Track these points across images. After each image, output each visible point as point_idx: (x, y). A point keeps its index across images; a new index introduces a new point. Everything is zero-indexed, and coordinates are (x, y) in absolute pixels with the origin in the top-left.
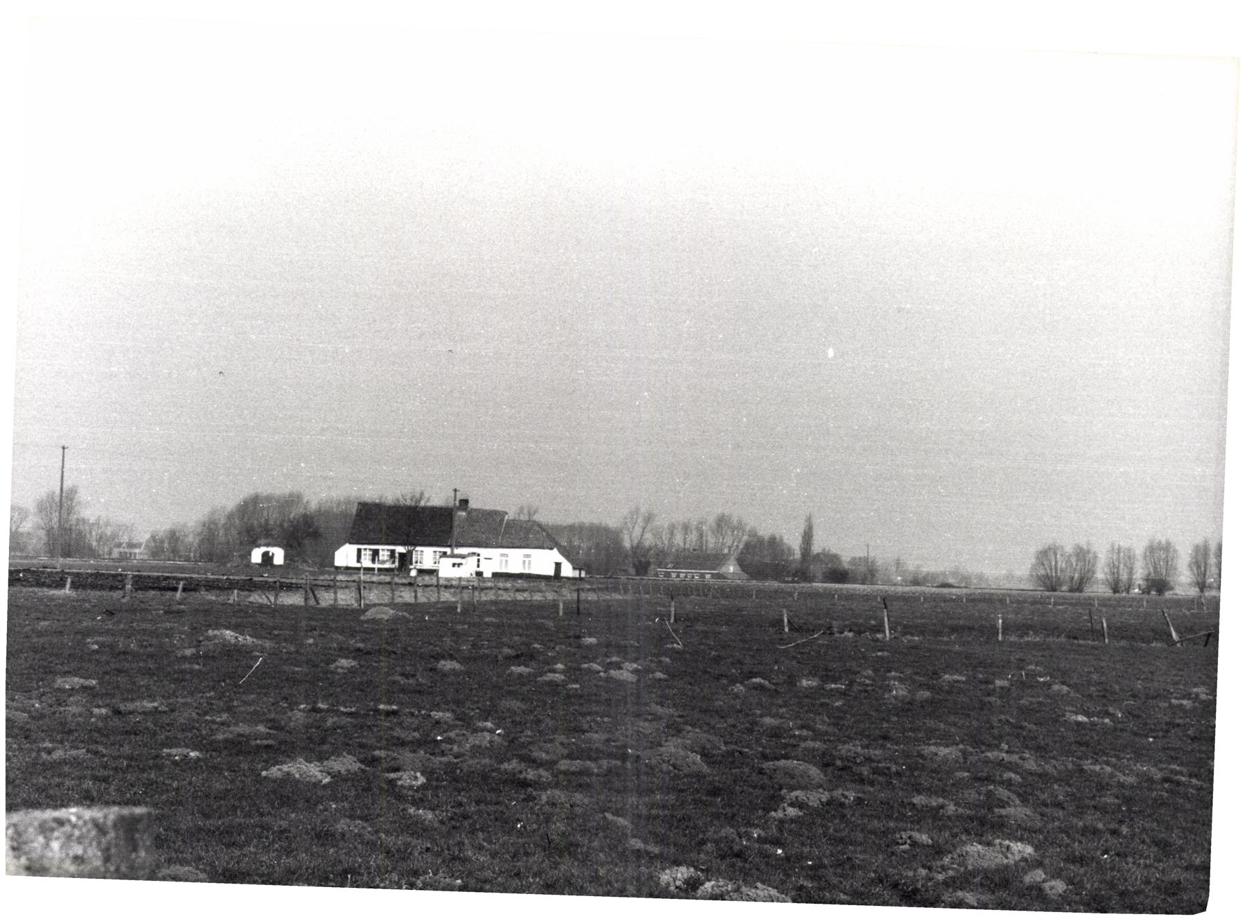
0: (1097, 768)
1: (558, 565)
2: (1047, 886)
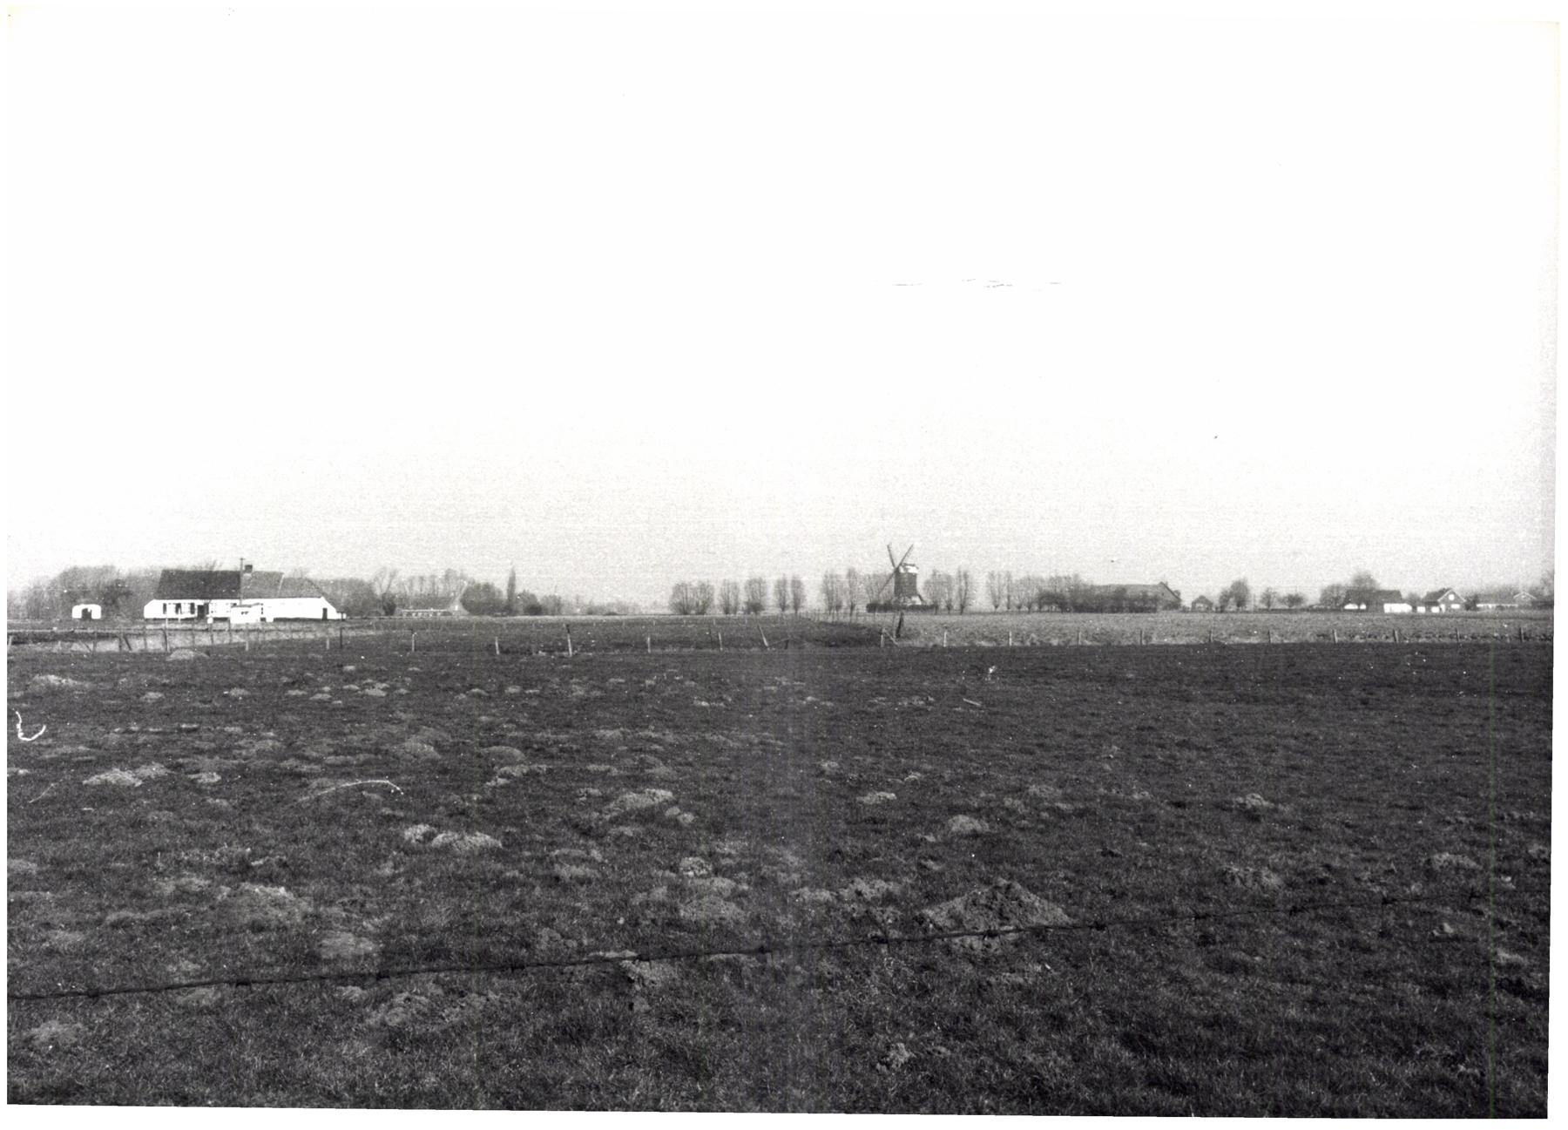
0: (715, 738)
1: (325, 610)
2: (680, 818)
